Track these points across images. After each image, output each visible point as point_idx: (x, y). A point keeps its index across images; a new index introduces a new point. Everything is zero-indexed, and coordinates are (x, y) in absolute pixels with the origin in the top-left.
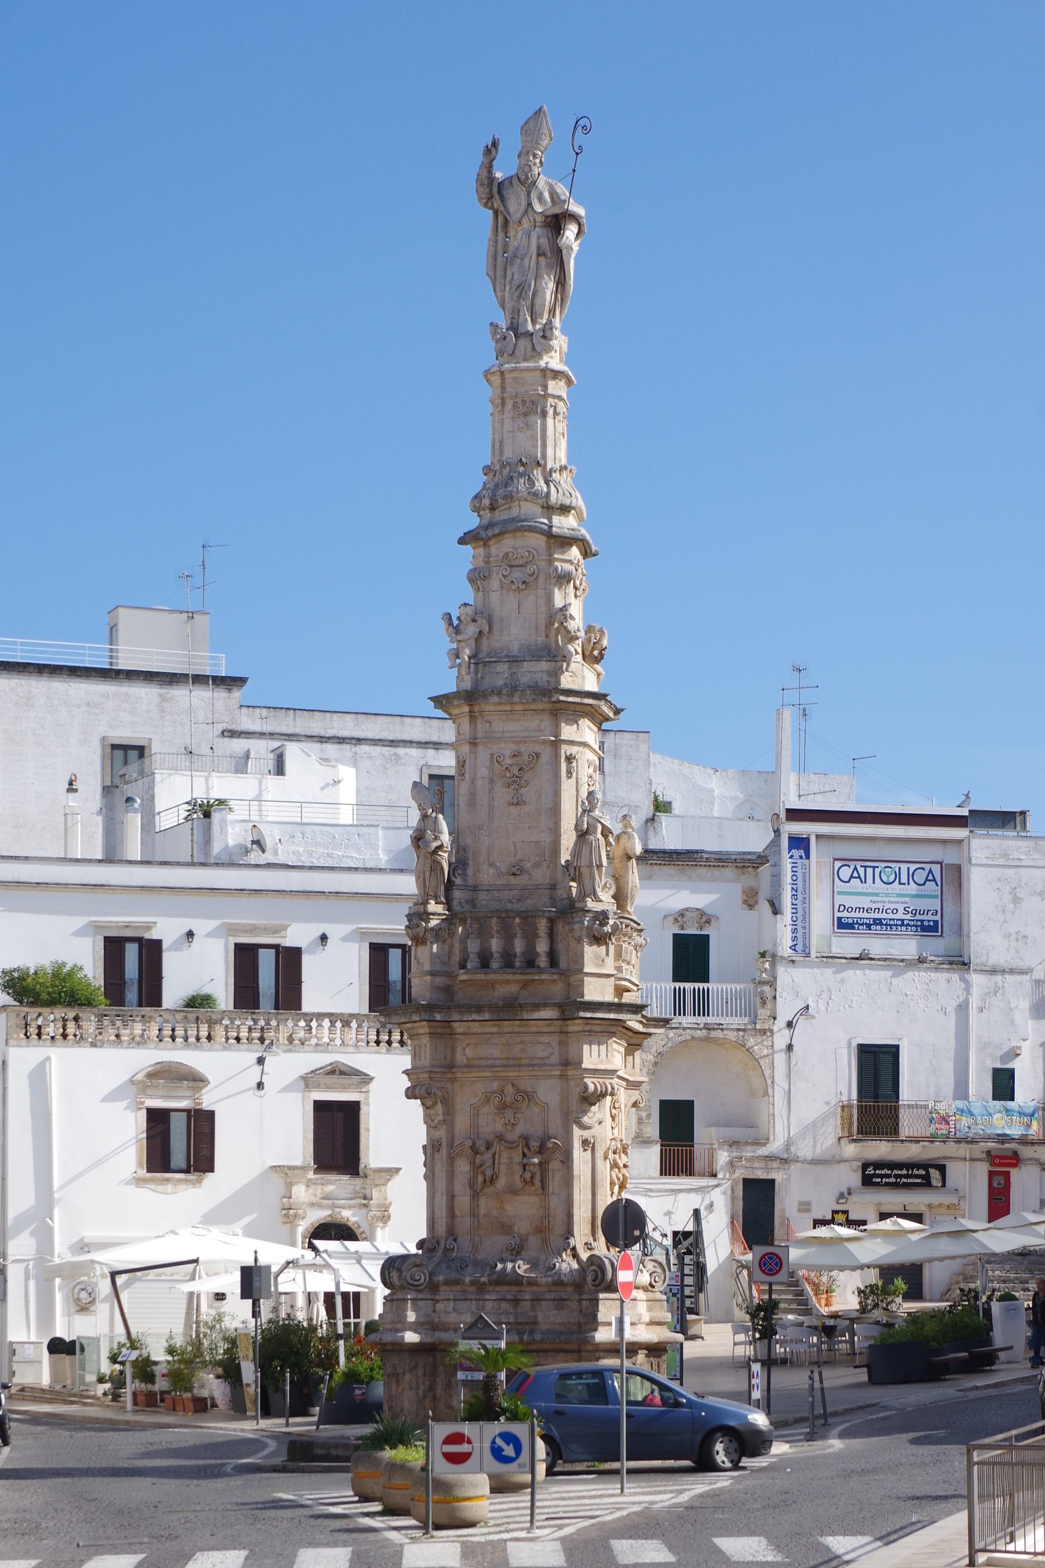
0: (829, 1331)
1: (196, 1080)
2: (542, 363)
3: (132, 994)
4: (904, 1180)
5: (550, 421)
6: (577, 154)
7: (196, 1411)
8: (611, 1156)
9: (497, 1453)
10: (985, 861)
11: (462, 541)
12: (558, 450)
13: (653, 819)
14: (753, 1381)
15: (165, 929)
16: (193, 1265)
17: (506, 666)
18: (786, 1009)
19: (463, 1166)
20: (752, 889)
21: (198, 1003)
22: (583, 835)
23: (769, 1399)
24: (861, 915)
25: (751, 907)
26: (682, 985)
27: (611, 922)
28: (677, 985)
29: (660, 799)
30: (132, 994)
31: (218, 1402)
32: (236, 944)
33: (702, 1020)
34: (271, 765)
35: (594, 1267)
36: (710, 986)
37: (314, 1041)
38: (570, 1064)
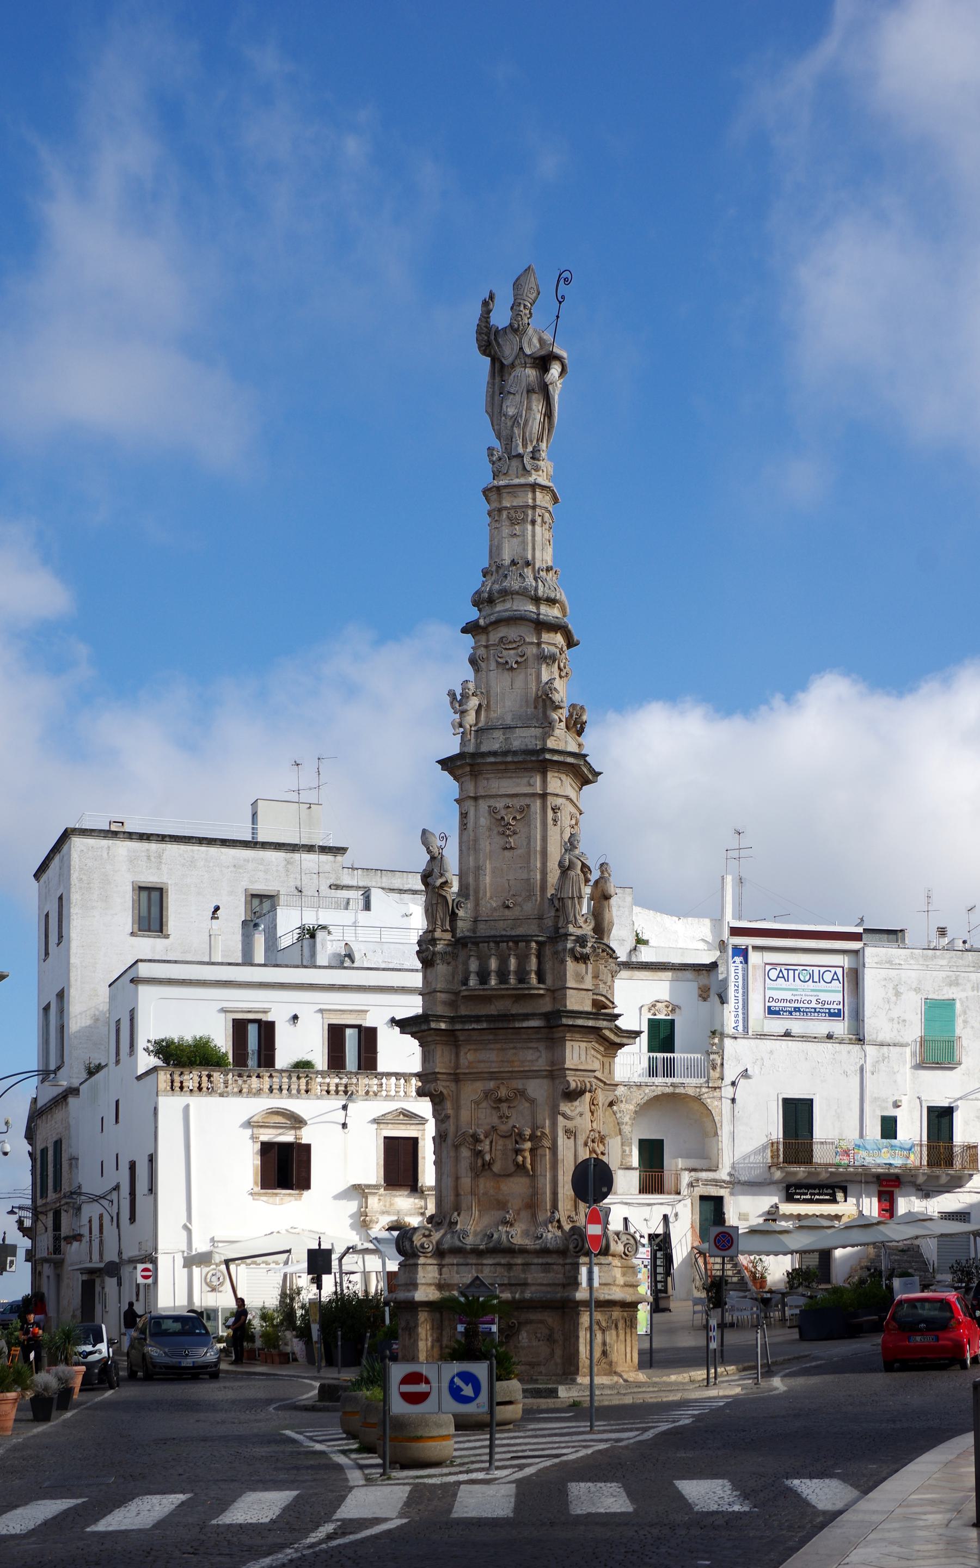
0: (766, 1302)
1: (297, 1122)
2: (531, 480)
3: (252, 1062)
4: (817, 1197)
5: (538, 528)
6: (560, 303)
7: (281, 1363)
8: (590, 1143)
9: (455, 1393)
10: (875, 965)
11: (464, 631)
12: (545, 554)
13: (635, 949)
14: (711, 1334)
15: (278, 1016)
16: (286, 1255)
17: (501, 732)
18: (730, 1075)
19: (465, 1153)
20: (705, 986)
21: (303, 1066)
22: (565, 870)
23: (722, 1351)
24: (785, 1004)
25: (705, 999)
26: (655, 1055)
27: (589, 945)
28: (651, 1054)
29: (640, 936)
30: (252, 1062)
31: (298, 1356)
32: (329, 1025)
33: (669, 1080)
34: (361, 904)
35: (575, 1237)
36: (675, 1055)
37: (384, 1093)
38: (556, 1072)
